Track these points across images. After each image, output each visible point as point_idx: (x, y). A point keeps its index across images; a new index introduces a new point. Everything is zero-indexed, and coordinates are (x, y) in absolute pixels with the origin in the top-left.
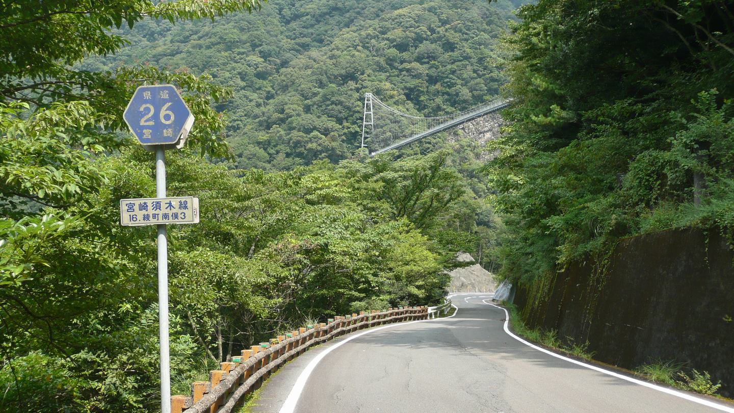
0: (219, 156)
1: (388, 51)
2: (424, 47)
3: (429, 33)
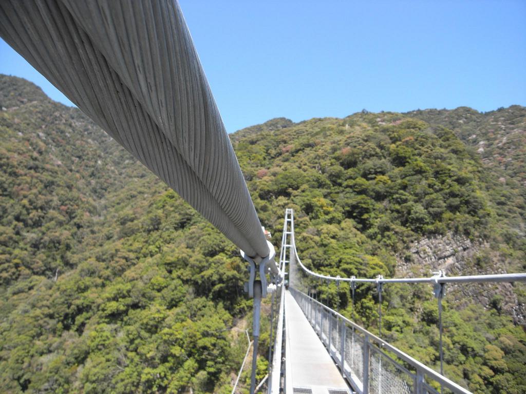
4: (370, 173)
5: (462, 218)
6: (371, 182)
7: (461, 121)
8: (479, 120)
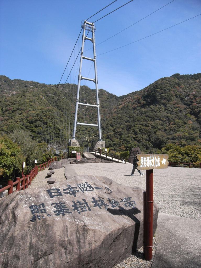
0: (17, 174)
1: (26, 124)
2: (38, 123)
3: (40, 119)
4: (37, 126)
5: (58, 139)
6: (37, 129)
7: (83, 92)
8: (89, 93)
